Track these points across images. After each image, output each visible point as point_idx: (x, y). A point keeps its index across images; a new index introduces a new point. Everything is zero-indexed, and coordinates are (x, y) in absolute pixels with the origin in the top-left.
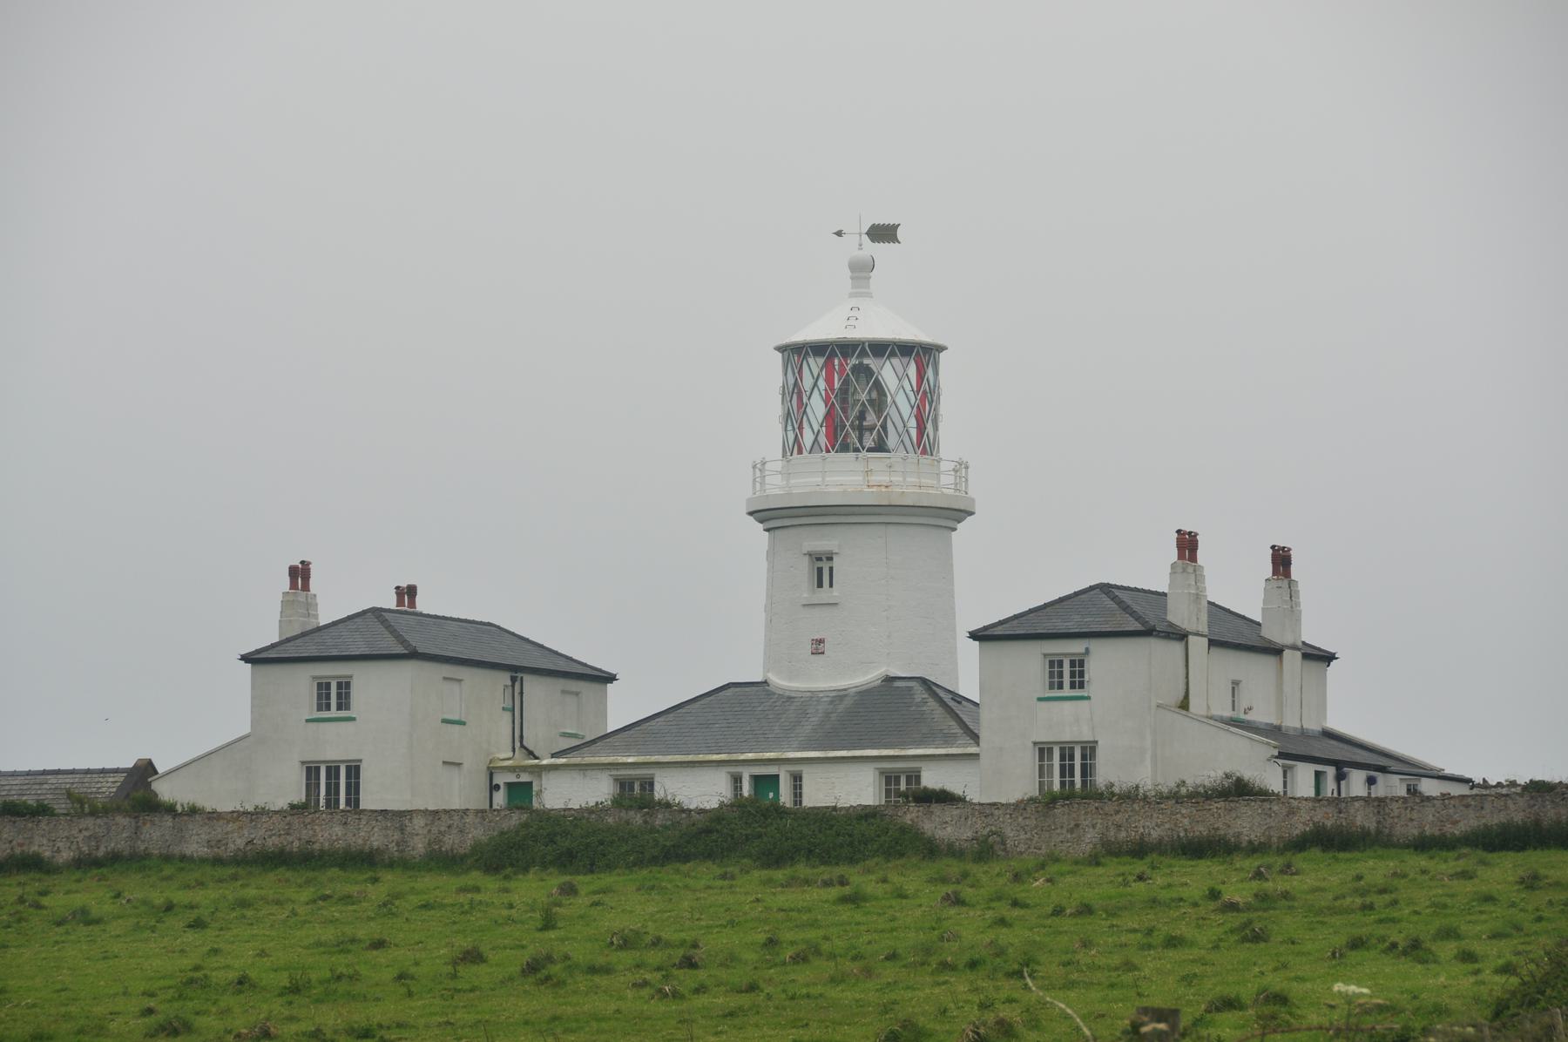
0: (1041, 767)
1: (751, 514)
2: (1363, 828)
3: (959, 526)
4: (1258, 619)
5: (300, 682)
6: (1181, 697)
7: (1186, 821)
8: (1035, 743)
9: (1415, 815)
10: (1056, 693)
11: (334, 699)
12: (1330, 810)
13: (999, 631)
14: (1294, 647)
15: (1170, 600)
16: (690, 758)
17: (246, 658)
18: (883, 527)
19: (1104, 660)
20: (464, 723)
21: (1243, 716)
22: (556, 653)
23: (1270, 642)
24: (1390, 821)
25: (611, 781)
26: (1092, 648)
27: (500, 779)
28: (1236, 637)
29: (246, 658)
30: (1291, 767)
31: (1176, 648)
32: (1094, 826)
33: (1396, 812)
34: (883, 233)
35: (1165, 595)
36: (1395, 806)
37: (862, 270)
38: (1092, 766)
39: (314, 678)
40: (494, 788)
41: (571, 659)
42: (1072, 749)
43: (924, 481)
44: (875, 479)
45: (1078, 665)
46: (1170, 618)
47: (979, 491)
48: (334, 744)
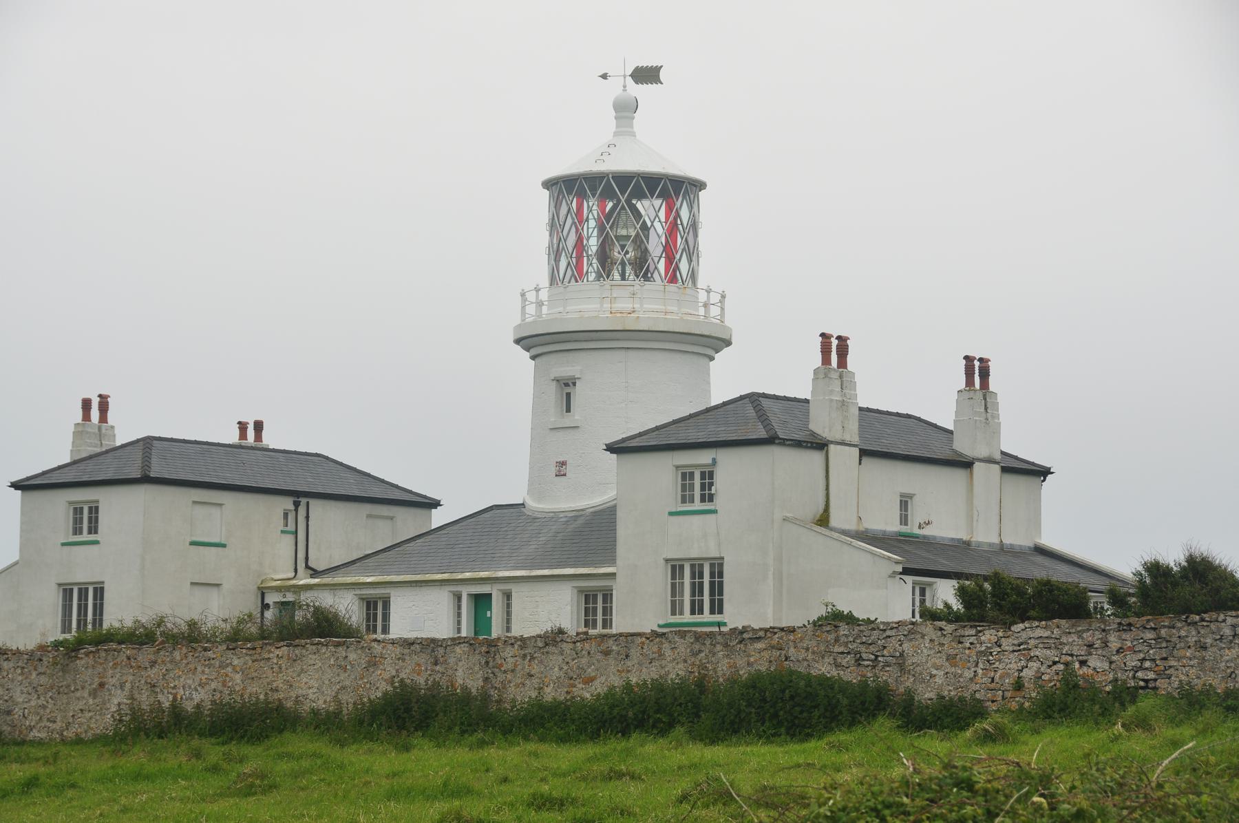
0: (673, 586)
1: (518, 341)
2: (465, 688)
3: (717, 356)
4: (951, 427)
5: (58, 505)
6: (821, 511)
7: (238, 678)
8: (667, 560)
9: (536, 668)
10: (688, 507)
11: (86, 521)
12: (423, 659)
13: (634, 443)
14: (989, 461)
15: (813, 408)
16: (418, 577)
17: (16, 485)
18: (623, 352)
19: (734, 470)
20: (224, 546)
21: (917, 531)
22: (383, 481)
23: (961, 455)
24: (501, 677)
26: (718, 460)
27: (271, 599)
28: (897, 442)
29: (16, 485)
30: (930, 584)
31: (816, 457)
32: (122, 687)
33: (509, 664)
34: (646, 75)
35: (807, 401)
36: (508, 652)
37: (626, 110)
38: (721, 584)
39: (70, 503)
41: (397, 487)
42: (701, 566)
43: (670, 308)
44: (618, 306)
45: (708, 476)
46: (812, 427)
47: (736, 322)
48: (84, 566)
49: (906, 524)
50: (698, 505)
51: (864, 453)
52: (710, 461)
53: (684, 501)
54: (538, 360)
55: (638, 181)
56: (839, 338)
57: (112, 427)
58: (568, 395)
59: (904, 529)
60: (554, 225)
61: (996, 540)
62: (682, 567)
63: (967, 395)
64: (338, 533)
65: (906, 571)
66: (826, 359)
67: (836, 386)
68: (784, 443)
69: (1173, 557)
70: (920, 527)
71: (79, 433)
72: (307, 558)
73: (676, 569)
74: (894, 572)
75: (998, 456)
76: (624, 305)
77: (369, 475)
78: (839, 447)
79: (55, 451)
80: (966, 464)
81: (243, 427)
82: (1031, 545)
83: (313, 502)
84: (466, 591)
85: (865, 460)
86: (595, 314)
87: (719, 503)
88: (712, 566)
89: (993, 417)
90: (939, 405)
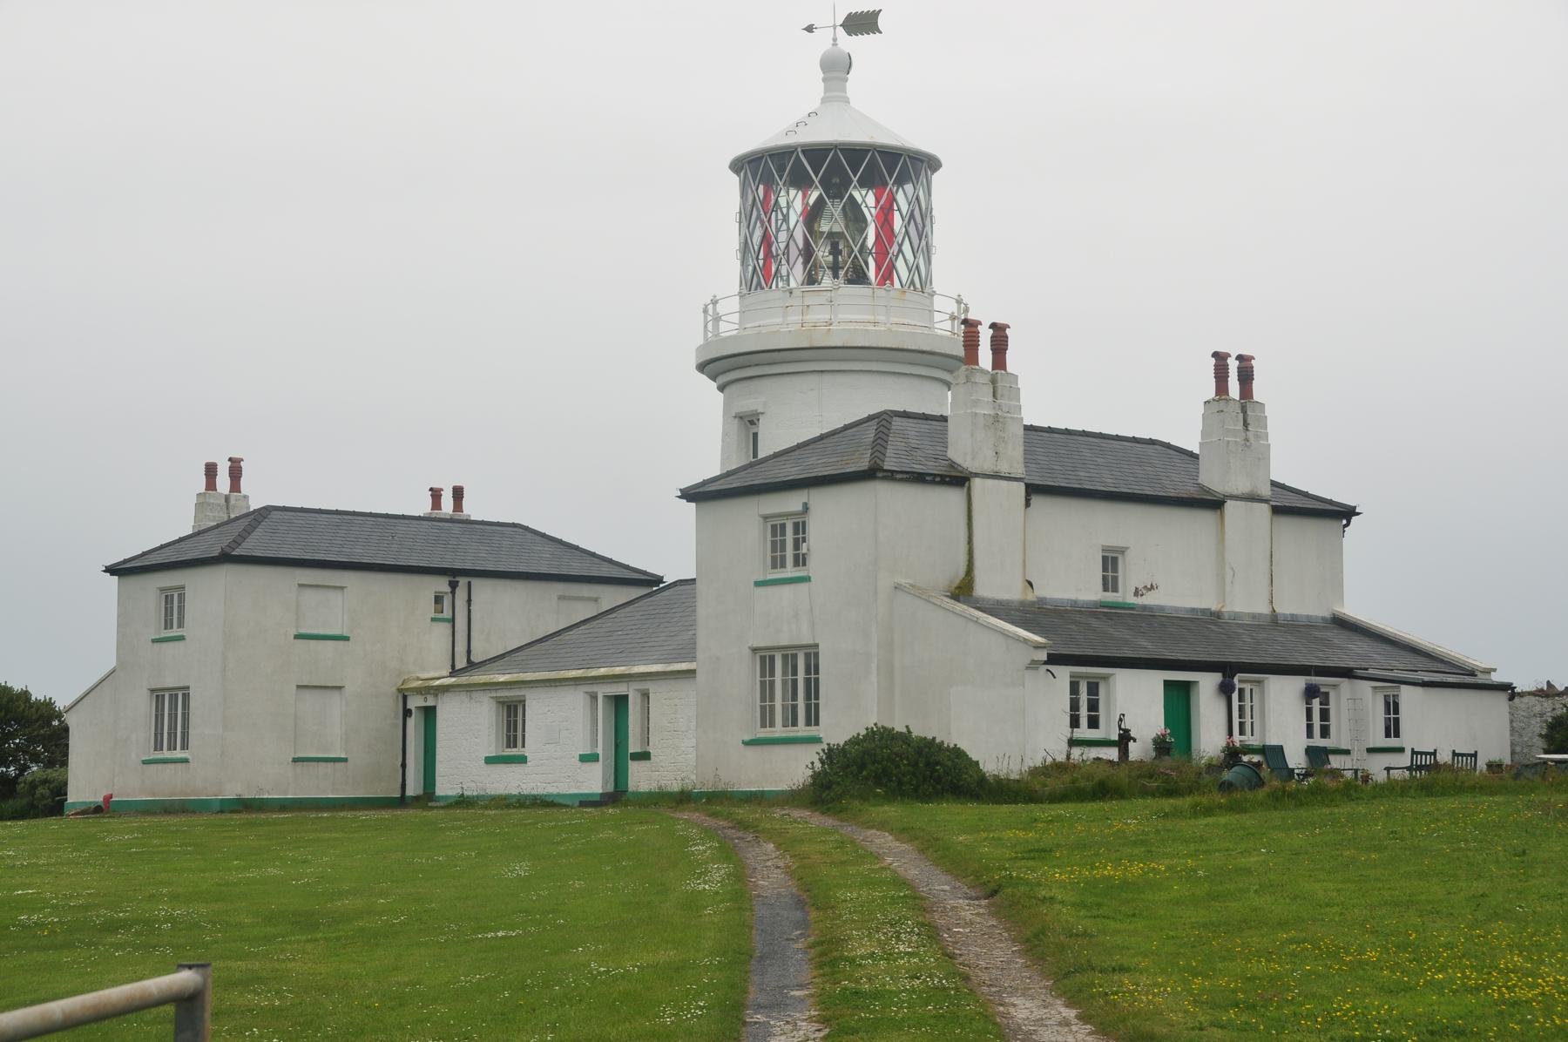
8: (755, 650)
17: (112, 570)
18: (816, 377)
19: (834, 517)
20: (347, 639)
21: (1132, 599)
22: (593, 555)
23: (1209, 491)
25: (493, 705)
29: (112, 570)
30: (1106, 678)
31: (952, 498)
34: (862, 23)
35: (944, 419)
37: (836, 68)
40: (407, 713)
41: (610, 561)
44: (811, 317)
46: (951, 454)
49: (1115, 590)
50: (790, 571)
51: (1032, 490)
52: (800, 508)
53: (774, 566)
54: (727, 390)
55: (836, 154)
56: (1240, 358)
57: (246, 497)
58: (755, 435)
59: (1110, 597)
60: (746, 217)
61: (1263, 609)
62: (772, 658)
63: (1215, 407)
65: (1054, 659)
67: (985, 394)
68: (891, 476)
69: (37, 694)
70: (1136, 593)
71: (202, 505)
72: (469, 652)
73: (765, 658)
74: (1033, 662)
75: (1266, 491)
76: (819, 315)
77: (577, 548)
78: (989, 482)
80: (1213, 504)
81: (436, 494)
82: (1327, 615)
83: (476, 582)
84: (603, 690)
85: (1035, 499)
86: (774, 329)
87: (814, 567)
88: (807, 656)
89: (1257, 437)
90: (1176, 416)
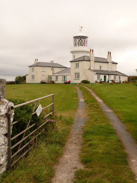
4: (106, 58)
14: (110, 62)
64: (57, 70)
66: (109, 54)
68: (85, 60)
79: (33, 63)
80: (108, 63)
